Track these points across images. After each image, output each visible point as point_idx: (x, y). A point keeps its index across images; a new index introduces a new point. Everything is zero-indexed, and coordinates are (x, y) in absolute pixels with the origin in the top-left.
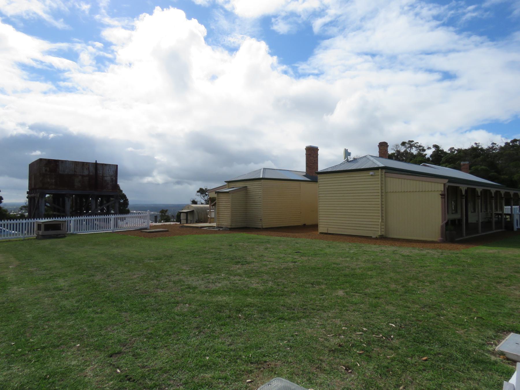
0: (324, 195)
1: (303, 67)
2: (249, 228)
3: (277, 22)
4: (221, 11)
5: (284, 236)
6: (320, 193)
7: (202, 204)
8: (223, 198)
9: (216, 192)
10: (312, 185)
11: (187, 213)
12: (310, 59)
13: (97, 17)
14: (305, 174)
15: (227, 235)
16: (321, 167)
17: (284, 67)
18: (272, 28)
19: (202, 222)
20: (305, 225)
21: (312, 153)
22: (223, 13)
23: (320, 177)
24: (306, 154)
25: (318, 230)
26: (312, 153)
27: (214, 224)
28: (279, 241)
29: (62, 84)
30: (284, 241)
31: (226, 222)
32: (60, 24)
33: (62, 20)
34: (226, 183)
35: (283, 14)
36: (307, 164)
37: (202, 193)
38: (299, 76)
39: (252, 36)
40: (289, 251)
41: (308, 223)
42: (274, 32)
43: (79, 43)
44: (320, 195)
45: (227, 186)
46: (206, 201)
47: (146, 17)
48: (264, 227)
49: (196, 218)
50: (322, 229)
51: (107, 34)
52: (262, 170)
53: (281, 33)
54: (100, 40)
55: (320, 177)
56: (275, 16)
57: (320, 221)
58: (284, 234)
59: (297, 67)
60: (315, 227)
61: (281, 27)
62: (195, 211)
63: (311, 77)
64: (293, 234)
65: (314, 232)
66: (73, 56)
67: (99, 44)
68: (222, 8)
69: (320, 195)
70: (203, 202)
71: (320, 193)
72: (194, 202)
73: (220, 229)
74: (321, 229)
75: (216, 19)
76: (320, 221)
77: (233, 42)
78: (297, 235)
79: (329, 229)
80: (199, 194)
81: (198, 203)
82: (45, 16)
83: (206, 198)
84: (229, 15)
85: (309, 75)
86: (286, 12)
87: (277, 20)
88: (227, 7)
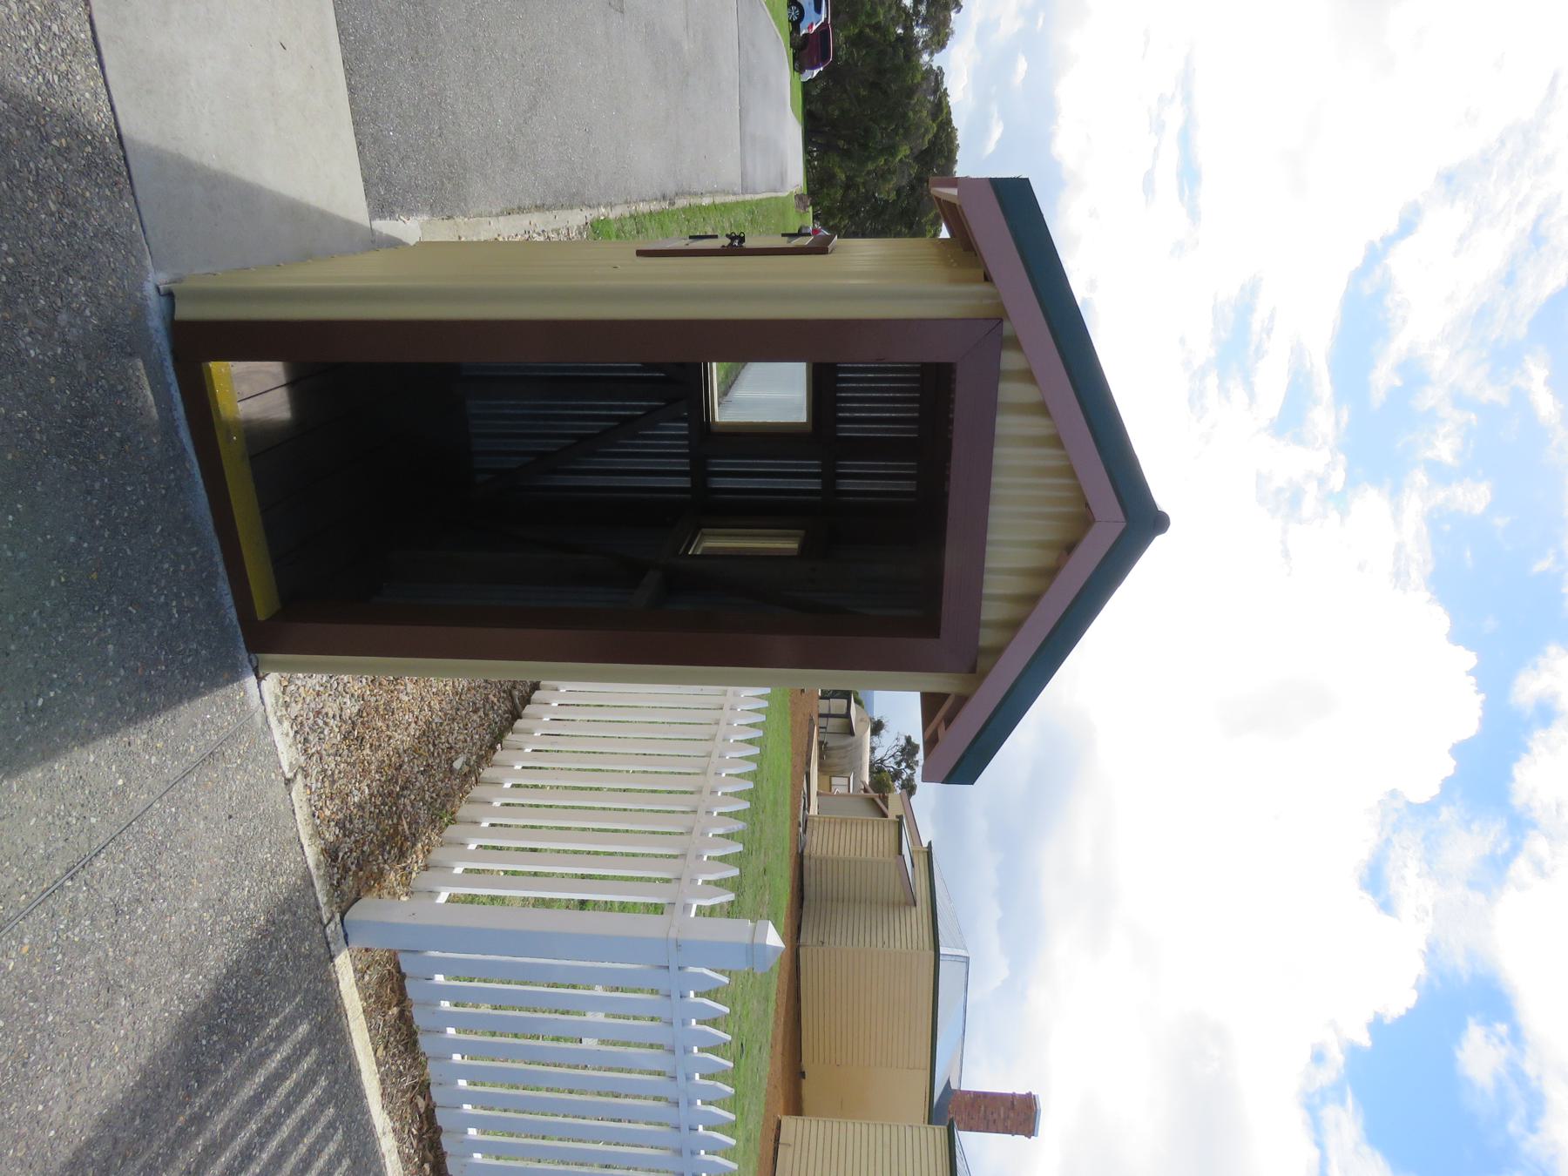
0: (887, 1139)
1: (1345, 1124)
2: (801, 906)
3: (1495, 1040)
4: (1506, 845)
5: (776, 1011)
6: (894, 1129)
7: (873, 750)
8: (886, 836)
9: (900, 817)
10: (921, 1111)
11: (848, 716)
12: (1378, 1156)
13: (1420, 477)
14: (954, 1086)
15: (787, 853)
16: (969, 1141)
17: (1337, 1057)
18: (1471, 1021)
19: (820, 757)
20: (803, 1075)
21: (1016, 1115)
22: (1499, 851)
23: (940, 1131)
24: (1013, 1095)
25: (787, 1113)
26: (1016, 1115)
27: (814, 810)
28: (767, 999)
29: (1212, 381)
30: (765, 1011)
31: (819, 844)
32: (1383, 377)
33: (1398, 382)
34: (925, 845)
35: (1530, 1068)
36: (985, 1095)
37: (903, 750)
38: (1313, 1106)
39: (1432, 951)
40: (746, 1027)
41: (807, 1086)
42: (1457, 1029)
43: (1337, 423)
44: (886, 1129)
45: (918, 848)
46: (882, 761)
47: (1439, 620)
48: (802, 951)
49: (833, 742)
50: (791, 1126)
51: (1371, 503)
52: (963, 953)
53: (1459, 1054)
54: (1351, 482)
55: (940, 1131)
56: (1516, 1036)
57: (814, 1123)
58: (782, 1011)
59: (1343, 1102)
60: (796, 1106)
61: (1479, 1056)
62: (851, 739)
63: (1314, 1153)
64: (780, 1038)
65: (781, 1104)
66: (1290, 422)
67: (1337, 480)
68: (1516, 849)
69: (886, 1129)
70: (879, 754)
71: (894, 1129)
72: (877, 728)
73: (802, 825)
74: (790, 1124)
75: (1475, 827)
76: (814, 1123)
77: (1403, 878)
78: (779, 1048)
79: (791, 1150)
80: (903, 742)
81: (875, 739)
82: (1399, 346)
83: (890, 764)
84: (1496, 868)
85: (1319, 1145)
86: (1539, 1078)
87: (1502, 1042)
88: (1521, 867)
